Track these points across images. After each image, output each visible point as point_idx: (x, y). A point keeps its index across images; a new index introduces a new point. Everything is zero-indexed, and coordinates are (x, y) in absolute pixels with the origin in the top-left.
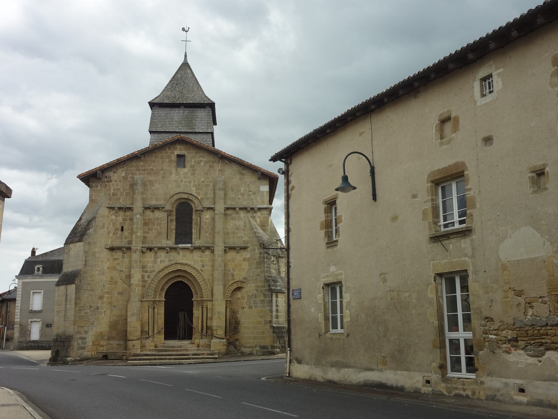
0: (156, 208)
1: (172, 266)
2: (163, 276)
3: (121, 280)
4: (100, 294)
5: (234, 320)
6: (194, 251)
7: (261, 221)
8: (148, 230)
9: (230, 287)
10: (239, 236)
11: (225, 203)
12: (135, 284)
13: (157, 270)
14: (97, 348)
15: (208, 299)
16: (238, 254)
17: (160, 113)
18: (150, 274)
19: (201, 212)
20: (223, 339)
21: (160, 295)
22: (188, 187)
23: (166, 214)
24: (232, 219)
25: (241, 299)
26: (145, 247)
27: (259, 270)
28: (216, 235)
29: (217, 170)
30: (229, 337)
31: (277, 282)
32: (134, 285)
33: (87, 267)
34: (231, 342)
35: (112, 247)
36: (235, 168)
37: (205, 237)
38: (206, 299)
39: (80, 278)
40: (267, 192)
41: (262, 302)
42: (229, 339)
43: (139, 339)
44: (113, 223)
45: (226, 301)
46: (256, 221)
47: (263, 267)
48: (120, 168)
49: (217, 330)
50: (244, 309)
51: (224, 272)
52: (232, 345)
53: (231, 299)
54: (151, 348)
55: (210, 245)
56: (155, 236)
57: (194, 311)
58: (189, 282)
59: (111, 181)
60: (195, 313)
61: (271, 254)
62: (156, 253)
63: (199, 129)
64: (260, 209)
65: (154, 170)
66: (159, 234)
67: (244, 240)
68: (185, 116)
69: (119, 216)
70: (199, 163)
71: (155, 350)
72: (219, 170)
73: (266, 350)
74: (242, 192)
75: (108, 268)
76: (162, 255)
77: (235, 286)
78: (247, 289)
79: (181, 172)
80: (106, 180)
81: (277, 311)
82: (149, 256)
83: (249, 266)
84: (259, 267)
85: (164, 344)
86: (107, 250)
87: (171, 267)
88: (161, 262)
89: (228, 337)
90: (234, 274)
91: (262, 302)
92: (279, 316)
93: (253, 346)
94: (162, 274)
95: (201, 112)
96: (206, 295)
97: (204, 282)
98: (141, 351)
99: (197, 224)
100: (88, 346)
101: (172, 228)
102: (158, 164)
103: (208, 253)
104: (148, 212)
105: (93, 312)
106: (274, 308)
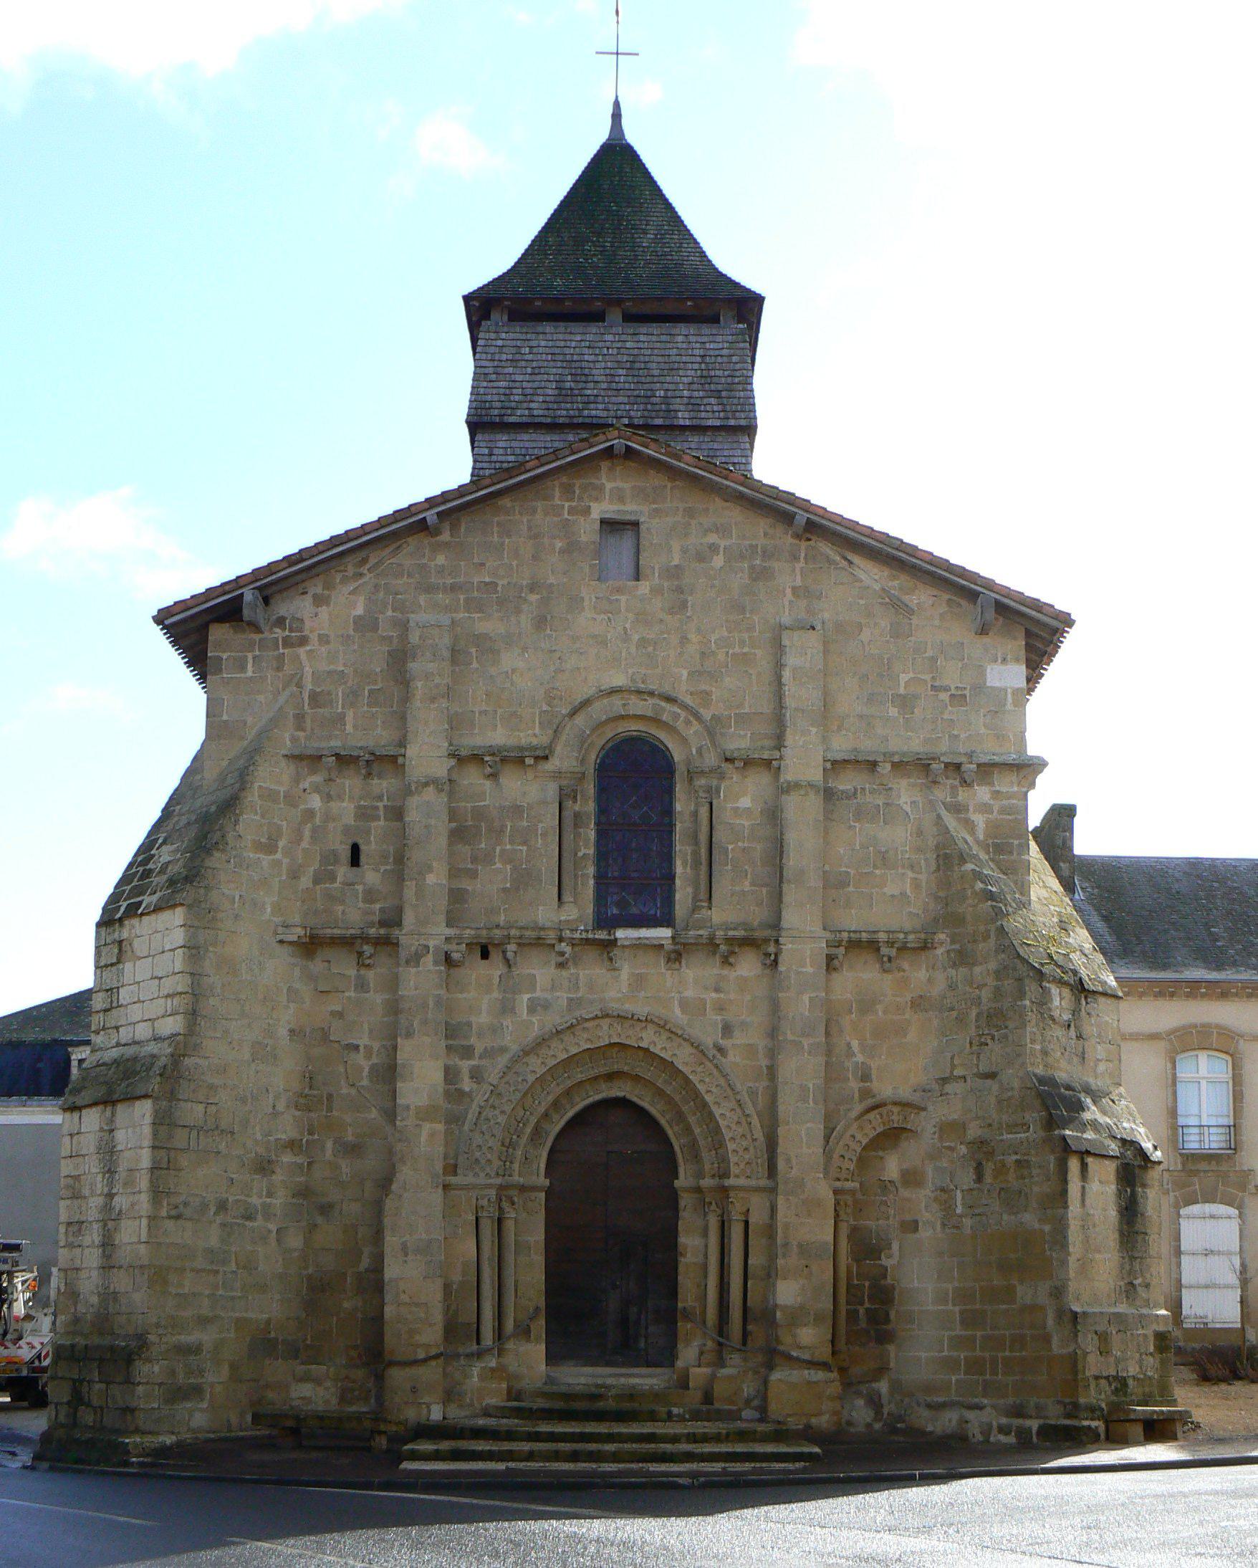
5: (867, 1284)
6: (684, 962)
13: (514, 1048)
15: (753, 1183)
18: (483, 1062)
24: (859, 815)
29: (789, 591)
44: (314, 831)
50: (916, 1229)
56: (504, 890)
65: (499, 589)
66: (523, 879)
69: (340, 798)
72: (794, 589)
77: (876, 1123)
86: (286, 950)
88: (532, 1009)
102: (514, 563)
103: (748, 966)
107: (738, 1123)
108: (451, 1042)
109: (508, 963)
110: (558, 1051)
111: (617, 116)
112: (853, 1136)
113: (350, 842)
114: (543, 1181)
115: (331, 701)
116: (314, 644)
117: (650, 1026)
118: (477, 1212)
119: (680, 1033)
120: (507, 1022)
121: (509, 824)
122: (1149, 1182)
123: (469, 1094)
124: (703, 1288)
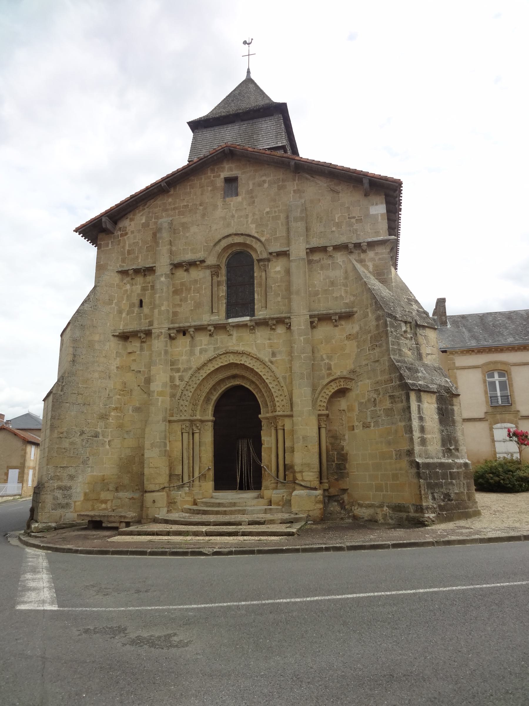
0: (192, 264)
1: (220, 358)
2: (205, 375)
3: (139, 388)
4: (101, 411)
5: (336, 453)
6: (256, 330)
7: (376, 266)
8: (181, 300)
10: (337, 297)
11: (308, 242)
13: (194, 367)
14: (93, 506)
15: (285, 413)
16: (337, 328)
17: (205, 134)
18: (184, 374)
19: (266, 263)
20: (315, 489)
21: (204, 410)
22: (244, 225)
23: (208, 272)
24: (322, 268)
25: (346, 411)
26: (173, 328)
27: (378, 350)
28: (294, 297)
29: (292, 192)
30: (327, 485)
31: (417, 371)
32: (156, 394)
33: (77, 365)
34: (332, 495)
35: (124, 333)
36: (323, 183)
37: (274, 303)
39: (62, 383)
40: (382, 215)
41: (389, 412)
42: (327, 490)
43: (164, 488)
44: (127, 297)
45: (319, 415)
46: (366, 267)
47: (384, 344)
48: (139, 212)
49: (304, 472)
50: (353, 430)
51: (312, 362)
52: (335, 501)
53: (327, 412)
54: (185, 507)
55: (283, 315)
56: (191, 310)
57: (262, 438)
58: (256, 390)
59: (126, 234)
60: (264, 441)
61: (400, 319)
62: (192, 338)
63: (263, 145)
64: (372, 245)
65: (189, 206)
66: (198, 305)
67: (346, 302)
68: (242, 132)
69: (136, 284)
70: (260, 185)
71: (189, 511)
72: (294, 191)
73: (404, 515)
74: (337, 221)
75: (117, 368)
76: (203, 339)
77: (334, 388)
78: (358, 392)
79: (232, 203)
80: (119, 233)
81: (422, 429)
82: (183, 342)
83: (358, 347)
84: (377, 346)
85: (212, 498)
86: (116, 339)
87: (218, 359)
88: (201, 353)
89: (326, 486)
91: (389, 412)
92: (427, 440)
93: (377, 503)
94: (204, 373)
95: (266, 122)
96: (281, 406)
97: (276, 383)
99: (260, 285)
100: (75, 502)
101: (220, 296)
102: (195, 197)
103: (281, 330)
104: (180, 273)
105: (88, 441)
106: (415, 423)
107: (279, 390)
108: (172, 367)
110: (211, 368)
111: (249, 72)
115: (134, 252)
116: (129, 235)
117: (244, 355)
119: (255, 357)
120: (192, 358)
121: (193, 287)
122: (455, 403)
123: (179, 386)
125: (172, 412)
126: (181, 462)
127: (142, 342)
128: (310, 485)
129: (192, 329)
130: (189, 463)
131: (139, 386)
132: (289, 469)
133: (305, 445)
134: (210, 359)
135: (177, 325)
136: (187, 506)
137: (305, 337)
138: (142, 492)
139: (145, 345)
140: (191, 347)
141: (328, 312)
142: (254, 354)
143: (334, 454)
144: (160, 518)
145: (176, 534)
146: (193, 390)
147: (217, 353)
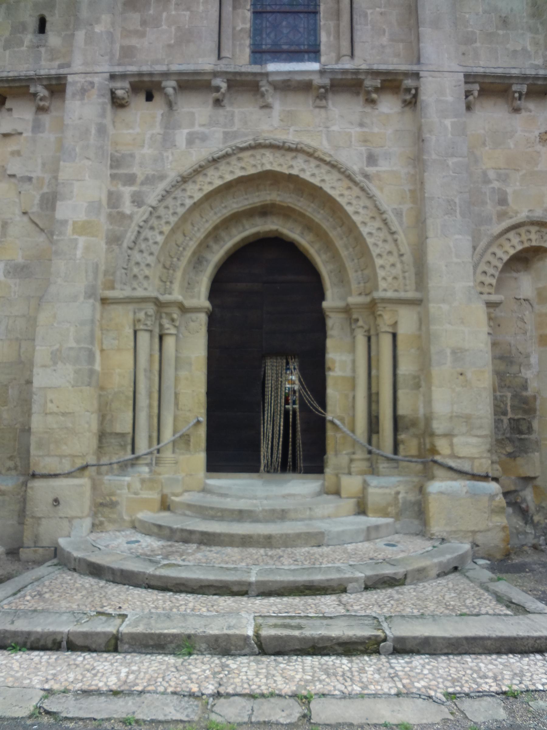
2: (198, 196)
3: (25, 219)
5: (509, 395)
6: (330, 102)
8: (144, 23)
9: (494, 249)
12: (75, 223)
13: (172, 175)
15: (402, 295)
16: (518, 116)
18: (145, 188)
26: (123, 76)
28: (426, 31)
38: (390, 294)
43: (84, 468)
56: (169, 46)
60: (334, 362)
71: (156, 530)
87: (233, 160)
88: (191, 140)
90: (505, 193)
96: (390, 279)
97: (378, 224)
98: (93, 525)
101: (238, 28)
107: (385, 241)
109: (170, 105)
112: (494, 254)
113: (37, 14)
114: (207, 304)
118: (135, 325)
120: (168, 154)
123: (131, 217)
124: (350, 399)
125: (111, 278)
126: (131, 402)
127: (41, 109)
128: (472, 469)
129: (173, 83)
130: (150, 406)
131: (25, 213)
132: (407, 428)
133: (459, 370)
134: (216, 156)
135: (133, 69)
136: (144, 515)
137: (456, 120)
138: (23, 475)
139: (46, 118)
140: (166, 128)
141: (507, 71)
142: (325, 154)
143: (506, 397)
144: (76, 554)
145: (146, 646)
146: (166, 229)
147: (230, 144)
